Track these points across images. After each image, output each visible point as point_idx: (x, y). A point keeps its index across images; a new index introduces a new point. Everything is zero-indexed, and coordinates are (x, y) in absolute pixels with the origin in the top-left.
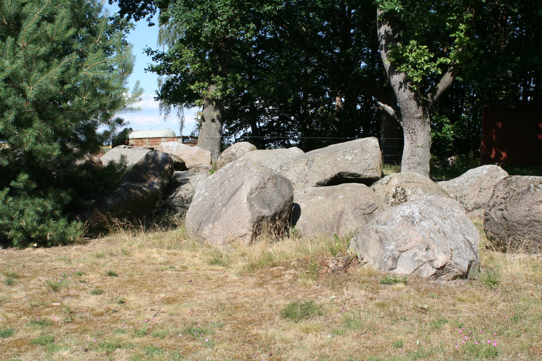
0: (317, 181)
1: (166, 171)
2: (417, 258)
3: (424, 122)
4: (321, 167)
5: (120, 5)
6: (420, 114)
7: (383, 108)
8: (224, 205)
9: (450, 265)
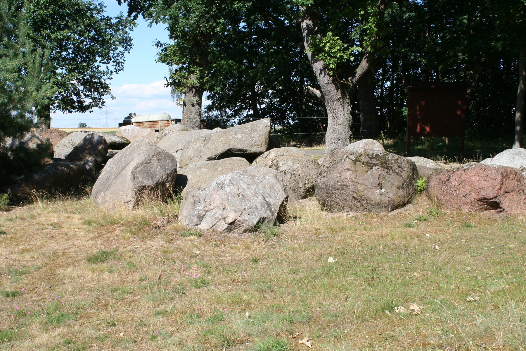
0: (209, 156)
1: (100, 151)
2: (215, 216)
3: (343, 103)
4: (214, 145)
5: (129, 5)
6: (339, 96)
7: (312, 91)
8: (115, 178)
9: (239, 221)
